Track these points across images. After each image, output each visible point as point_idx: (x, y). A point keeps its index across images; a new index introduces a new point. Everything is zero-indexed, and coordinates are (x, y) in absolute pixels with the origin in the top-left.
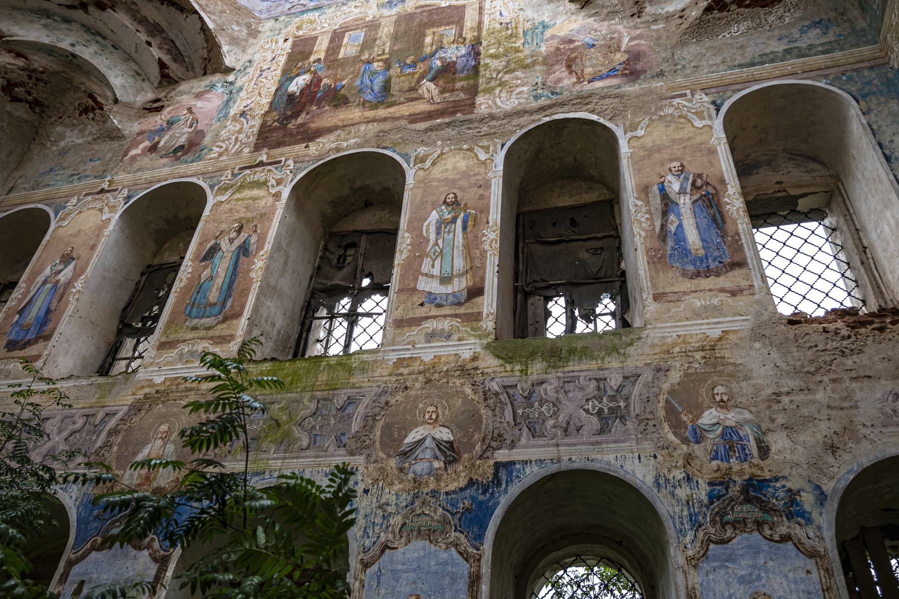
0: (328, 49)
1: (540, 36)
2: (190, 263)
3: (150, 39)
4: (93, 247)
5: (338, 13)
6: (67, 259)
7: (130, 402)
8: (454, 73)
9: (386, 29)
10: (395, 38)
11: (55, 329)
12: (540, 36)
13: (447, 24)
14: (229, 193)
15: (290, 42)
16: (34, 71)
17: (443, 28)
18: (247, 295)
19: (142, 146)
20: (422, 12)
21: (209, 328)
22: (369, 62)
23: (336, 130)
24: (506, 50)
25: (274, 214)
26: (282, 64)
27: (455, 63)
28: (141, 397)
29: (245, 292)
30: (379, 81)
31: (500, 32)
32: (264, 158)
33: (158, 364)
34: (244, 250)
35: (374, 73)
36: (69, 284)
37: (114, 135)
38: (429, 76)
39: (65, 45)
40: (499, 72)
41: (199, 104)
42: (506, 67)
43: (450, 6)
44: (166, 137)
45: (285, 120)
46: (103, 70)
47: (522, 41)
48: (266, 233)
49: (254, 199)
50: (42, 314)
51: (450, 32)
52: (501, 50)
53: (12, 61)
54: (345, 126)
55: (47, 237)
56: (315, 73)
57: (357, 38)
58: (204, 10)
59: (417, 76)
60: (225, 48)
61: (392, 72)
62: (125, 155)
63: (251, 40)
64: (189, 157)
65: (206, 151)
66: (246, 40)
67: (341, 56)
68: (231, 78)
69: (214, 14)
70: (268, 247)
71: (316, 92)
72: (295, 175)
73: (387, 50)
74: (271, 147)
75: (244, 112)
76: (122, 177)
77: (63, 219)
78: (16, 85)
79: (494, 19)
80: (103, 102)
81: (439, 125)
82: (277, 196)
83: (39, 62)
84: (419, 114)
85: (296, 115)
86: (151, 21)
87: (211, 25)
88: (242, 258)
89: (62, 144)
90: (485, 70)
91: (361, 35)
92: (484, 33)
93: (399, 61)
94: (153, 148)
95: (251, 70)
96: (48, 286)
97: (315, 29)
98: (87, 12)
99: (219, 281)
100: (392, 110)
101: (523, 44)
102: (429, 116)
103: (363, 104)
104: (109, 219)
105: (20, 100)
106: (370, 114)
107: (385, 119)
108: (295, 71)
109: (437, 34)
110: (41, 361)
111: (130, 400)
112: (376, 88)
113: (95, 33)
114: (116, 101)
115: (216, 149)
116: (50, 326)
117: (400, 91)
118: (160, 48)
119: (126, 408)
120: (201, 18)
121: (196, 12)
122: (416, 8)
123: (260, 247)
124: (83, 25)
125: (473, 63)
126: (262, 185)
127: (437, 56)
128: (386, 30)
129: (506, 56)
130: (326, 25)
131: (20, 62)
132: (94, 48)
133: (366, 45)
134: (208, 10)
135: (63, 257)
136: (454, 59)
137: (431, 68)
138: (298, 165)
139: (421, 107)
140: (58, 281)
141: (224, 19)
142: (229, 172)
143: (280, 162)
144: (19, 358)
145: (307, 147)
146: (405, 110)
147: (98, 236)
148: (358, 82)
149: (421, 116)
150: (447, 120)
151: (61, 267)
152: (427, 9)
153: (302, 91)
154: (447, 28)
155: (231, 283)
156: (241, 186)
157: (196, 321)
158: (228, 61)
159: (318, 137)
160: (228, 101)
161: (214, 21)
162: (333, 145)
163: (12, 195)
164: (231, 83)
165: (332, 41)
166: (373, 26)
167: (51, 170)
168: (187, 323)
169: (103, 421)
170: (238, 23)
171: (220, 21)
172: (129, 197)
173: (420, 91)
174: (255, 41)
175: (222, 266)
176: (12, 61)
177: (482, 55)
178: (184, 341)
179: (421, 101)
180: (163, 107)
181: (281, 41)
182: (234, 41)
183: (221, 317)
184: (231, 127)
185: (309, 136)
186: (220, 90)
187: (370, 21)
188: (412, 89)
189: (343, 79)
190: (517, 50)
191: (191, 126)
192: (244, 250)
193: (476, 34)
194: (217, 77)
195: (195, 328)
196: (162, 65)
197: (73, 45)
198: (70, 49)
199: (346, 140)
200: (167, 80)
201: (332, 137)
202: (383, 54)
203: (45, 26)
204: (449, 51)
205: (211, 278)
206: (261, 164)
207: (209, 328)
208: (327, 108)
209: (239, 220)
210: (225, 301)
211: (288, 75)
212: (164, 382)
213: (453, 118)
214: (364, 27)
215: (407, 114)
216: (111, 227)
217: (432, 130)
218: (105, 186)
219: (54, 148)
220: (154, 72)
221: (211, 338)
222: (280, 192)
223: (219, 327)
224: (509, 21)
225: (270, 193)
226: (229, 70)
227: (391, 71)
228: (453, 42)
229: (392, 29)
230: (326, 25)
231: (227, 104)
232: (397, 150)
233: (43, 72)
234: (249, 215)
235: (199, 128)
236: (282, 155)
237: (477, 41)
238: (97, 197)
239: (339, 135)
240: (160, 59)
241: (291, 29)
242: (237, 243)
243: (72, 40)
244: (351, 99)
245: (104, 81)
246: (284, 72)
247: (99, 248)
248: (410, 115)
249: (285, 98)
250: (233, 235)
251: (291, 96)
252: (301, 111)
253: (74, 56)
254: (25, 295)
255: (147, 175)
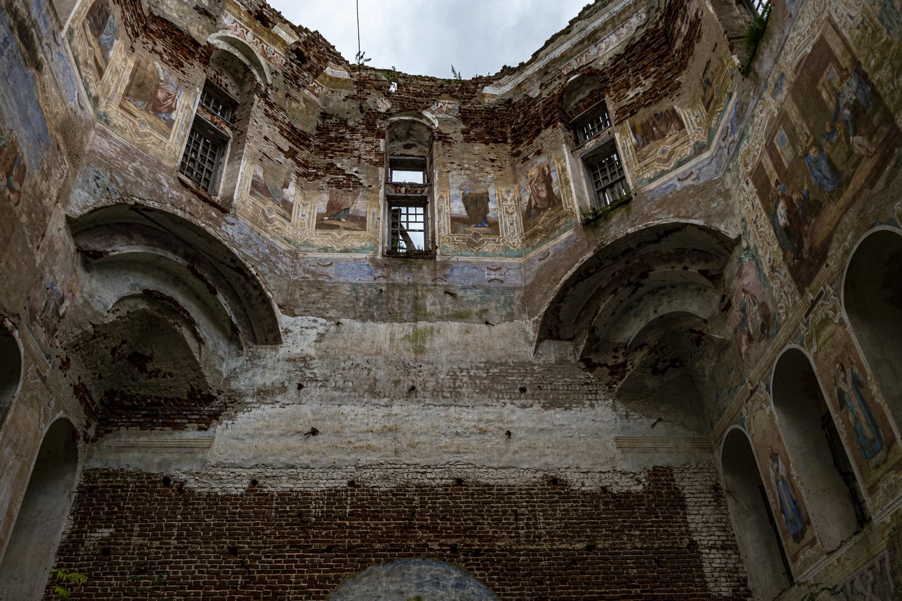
0: (774, 165)
1: (893, 12)
2: (837, 416)
3: (683, 265)
4: (779, 439)
5: (756, 128)
6: (774, 457)
7: (885, 546)
8: (864, 112)
9: (792, 112)
10: (804, 115)
11: (807, 516)
12: (893, 12)
13: (825, 67)
14: (814, 343)
15: (751, 183)
16: (655, 347)
17: (825, 73)
18: (887, 420)
19: (743, 342)
20: (802, 73)
21: (885, 461)
22: (806, 154)
23: (832, 236)
24: (882, 53)
25: (851, 339)
26: (760, 206)
27: (856, 101)
28: (888, 538)
29: (883, 416)
30: (823, 164)
31: (863, 37)
32: (811, 297)
33: (878, 507)
34: (858, 384)
35: (816, 161)
36: (789, 475)
37: (724, 346)
38: (851, 131)
39: (653, 317)
40: (893, 82)
41: (745, 281)
42: (893, 69)
43: (814, 47)
44: (750, 324)
45: (798, 251)
46: (681, 309)
47: (885, 31)
48: (859, 359)
49: (832, 336)
50: (793, 507)
51: (831, 73)
52: (877, 55)
53: (642, 355)
54: (835, 227)
55: (753, 448)
56: (783, 196)
57: (782, 138)
58: (689, 218)
59: (843, 139)
60: (722, 228)
61: (826, 150)
62: (741, 355)
63: (731, 202)
64: (772, 331)
65: (777, 318)
66: (728, 205)
67: (786, 166)
68: (744, 244)
69: (696, 213)
70: (868, 370)
71: (797, 213)
72: (839, 297)
73: (808, 132)
74: (809, 284)
75: (772, 267)
76: (753, 374)
77: (750, 429)
78: (656, 364)
79: (851, 28)
80: (700, 329)
81: (892, 171)
82: (842, 322)
83: (652, 339)
84: (871, 174)
85: (801, 245)
86: (673, 252)
87: (701, 222)
88: (861, 390)
89: (707, 373)
90: (882, 88)
91: (782, 132)
92: (854, 50)
93: (823, 136)
94: (750, 339)
95: (749, 228)
96: (780, 483)
97: (755, 157)
98: (643, 286)
99: (862, 418)
100: (851, 187)
101: (888, 33)
102: (878, 170)
103: (831, 197)
104: (771, 412)
105: (666, 369)
106: (841, 203)
107: (854, 199)
108: (772, 205)
109: (826, 83)
110: (818, 541)
111: (883, 544)
112: (828, 175)
113: (657, 291)
114: (705, 321)
115: (781, 311)
116: (803, 514)
117: (844, 163)
118: (693, 263)
119: (886, 551)
120: (692, 225)
121: (686, 224)
122: (795, 72)
123: (865, 375)
124: (648, 293)
125: (869, 89)
126: (826, 321)
127: (841, 106)
128: (794, 113)
129: (885, 58)
130: (758, 146)
131: (646, 351)
132: (665, 300)
133: (793, 140)
134: (690, 214)
135: (771, 457)
136: (854, 97)
137: (846, 121)
138: (835, 286)
139: (867, 166)
140: (782, 477)
141: (703, 208)
142: (801, 324)
143: (822, 293)
144: (806, 545)
145: (827, 266)
146: (859, 180)
147: (775, 428)
148: (814, 180)
149: (873, 175)
150: (893, 163)
151: (775, 465)
152: (802, 66)
153: (789, 218)
154: (828, 70)
155: (870, 415)
156: (817, 331)
157: (874, 459)
158: (732, 234)
159: (827, 251)
160: (757, 264)
161: (700, 217)
162: (841, 251)
163: (715, 428)
164: (748, 248)
165: (772, 157)
166: (783, 118)
167: (718, 396)
168: (870, 465)
169: (882, 568)
170: (713, 200)
171: (703, 213)
172: (767, 387)
173: (856, 152)
174: (733, 200)
175: (854, 402)
176: (642, 355)
177: (870, 75)
178: (879, 480)
179: (863, 160)
180: (730, 301)
181: (745, 186)
182: (723, 216)
183: (885, 447)
184: (775, 285)
185: (821, 255)
186: (747, 260)
187: (779, 115)
188: (850, 154)
189: (802, 186)
190: (888, 44)
191: (755, 304)
192: (858, 384)
193: (849, 56)
194: (737, 251)
195: (877, 467)
196: (703, 273)
197: (655, 312)
198: (656, 316)
199: (845, 240)
200: (715, 278)
201: (835, 244)
202: (808, 137)
203: (636, 316)
204: (846, 93)
205: (857, 419)
206: (814, 303)
207: (885, 461)
208: (813, 221)
209: (836, 361)
210: (878, 432)
211: (772, 216)
212: (892, 519)
213: (896, 157)
214: (779, 125)
215: (863, 181)
216: (777, 418)
217: (890, 181)
218: (750, 388)
219: (706, 379)
220: (704, 280)
221: (892, 469)
222: (841, 319)
223: (890, 456)
224: (861, 19)
225: (836, 324)
226: (739, 240)
227: (825, 149)
228: (842, 81)
229: (796, 108)
230: (758, 146)
231: (759, 269)
232: (882, 221)
233: (659, 343)
234: (839, 352)
235: (760, 302)
236: (818, 285)
237: (856, 63)
238: (752, 399)
239: (838, 239)
240: (700, 271)
241: (742, 170)
242: (849, 380)
243: (652, 309)
244: (821, 200)
245: (690, 315)
246: (767, 211)
247: (783, 438)
248: (866, 180)
249: (784, 233)
250: (842, 375)
251: (786, 229)
252: (801, 238)
253: (662, 317)
254: (774, 495)
255: (762, 363)
